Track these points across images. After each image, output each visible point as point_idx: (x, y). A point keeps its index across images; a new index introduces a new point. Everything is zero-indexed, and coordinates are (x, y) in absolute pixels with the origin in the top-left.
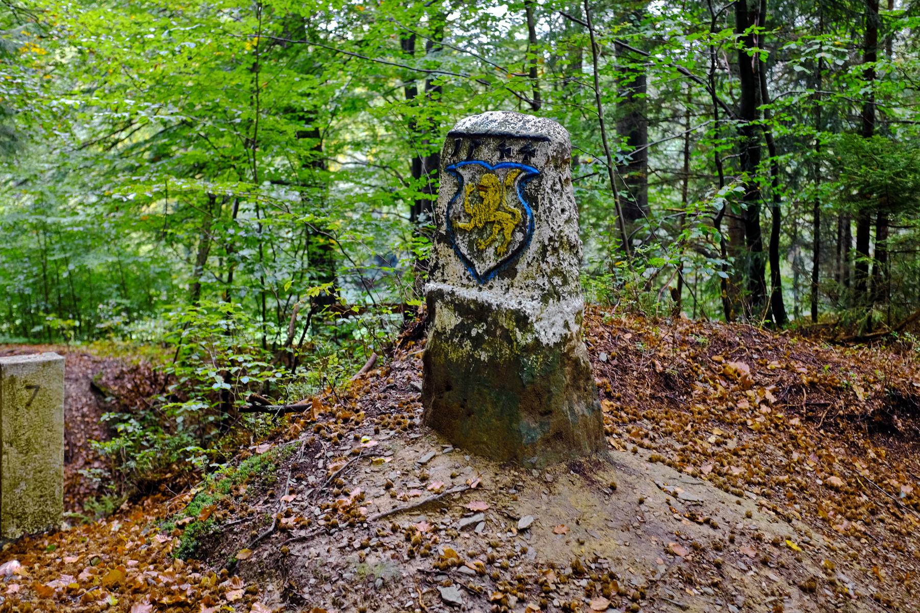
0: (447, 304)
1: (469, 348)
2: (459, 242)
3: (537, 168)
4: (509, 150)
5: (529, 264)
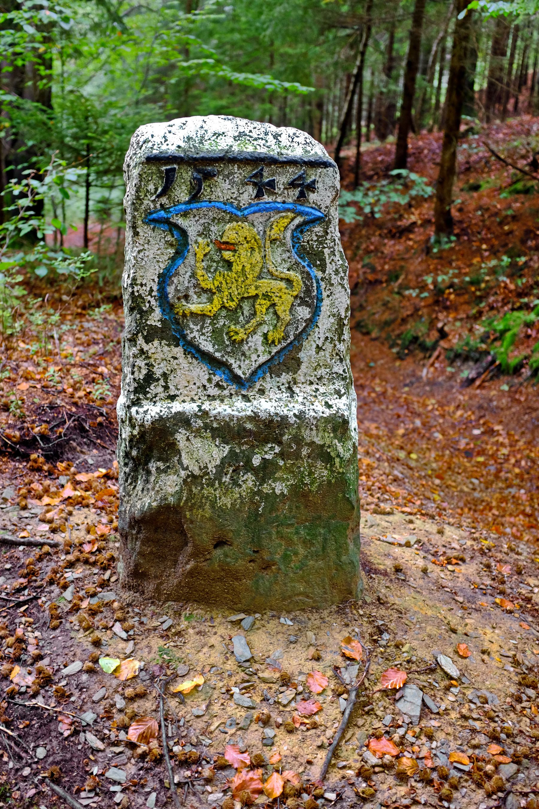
0: (198, 433)
1: (250, 484)
2: (196, 334)
3: (320, 209)
4: (272, 184)
5: (319, 348)
